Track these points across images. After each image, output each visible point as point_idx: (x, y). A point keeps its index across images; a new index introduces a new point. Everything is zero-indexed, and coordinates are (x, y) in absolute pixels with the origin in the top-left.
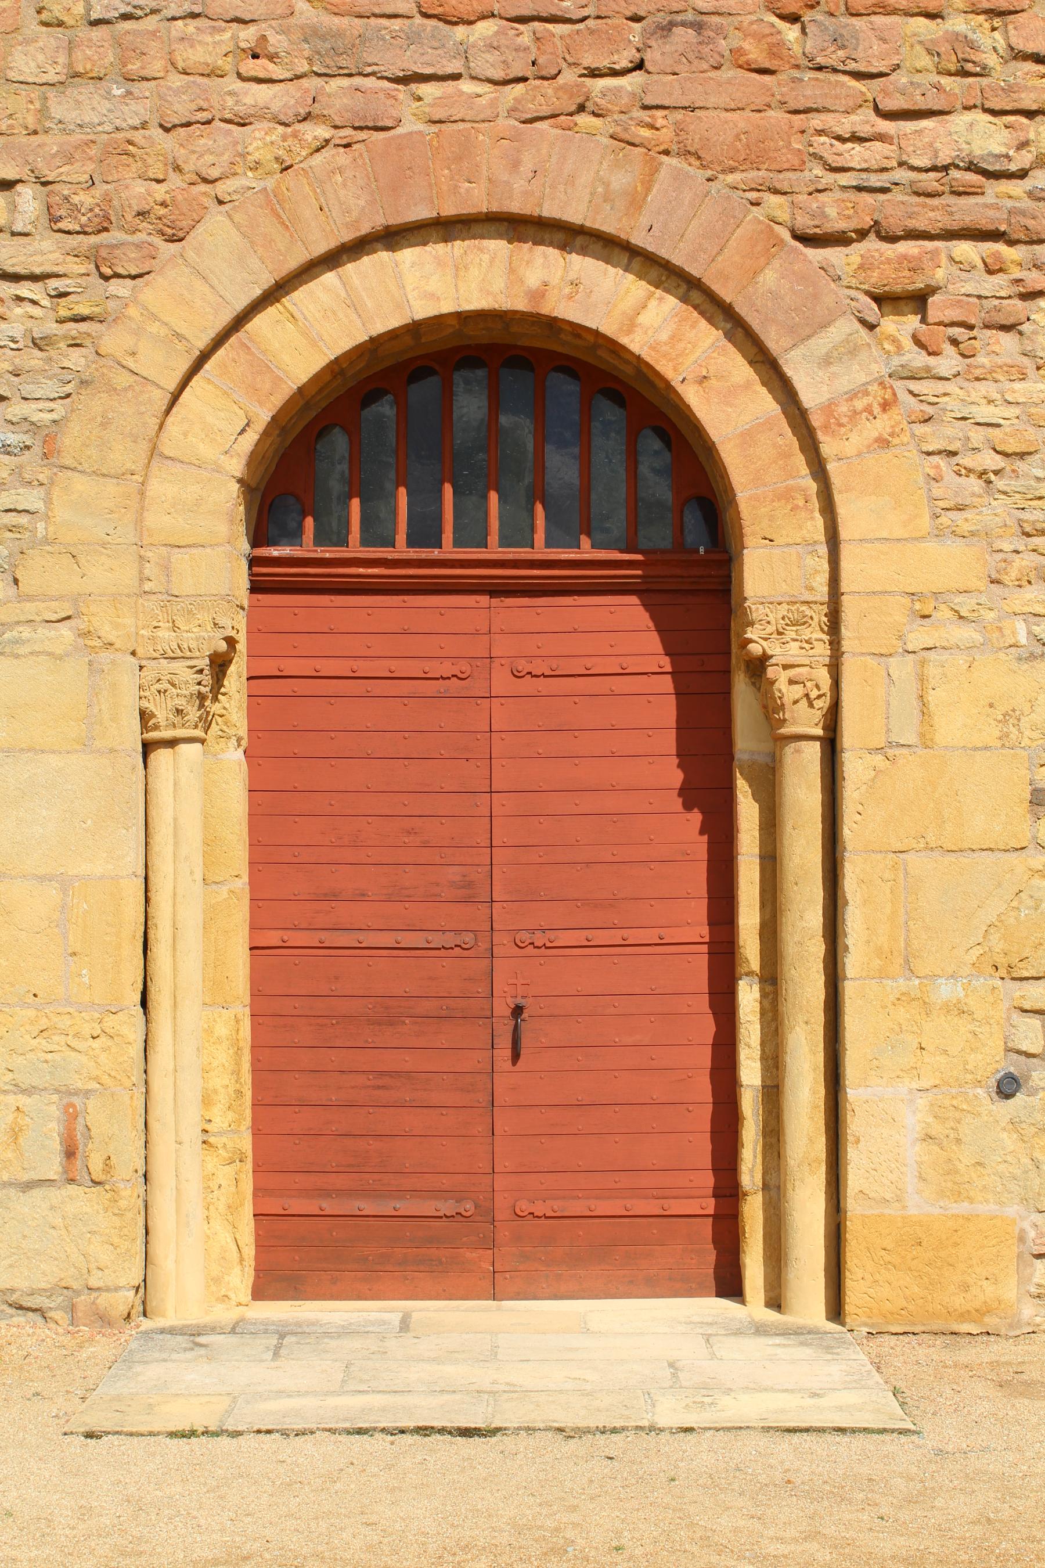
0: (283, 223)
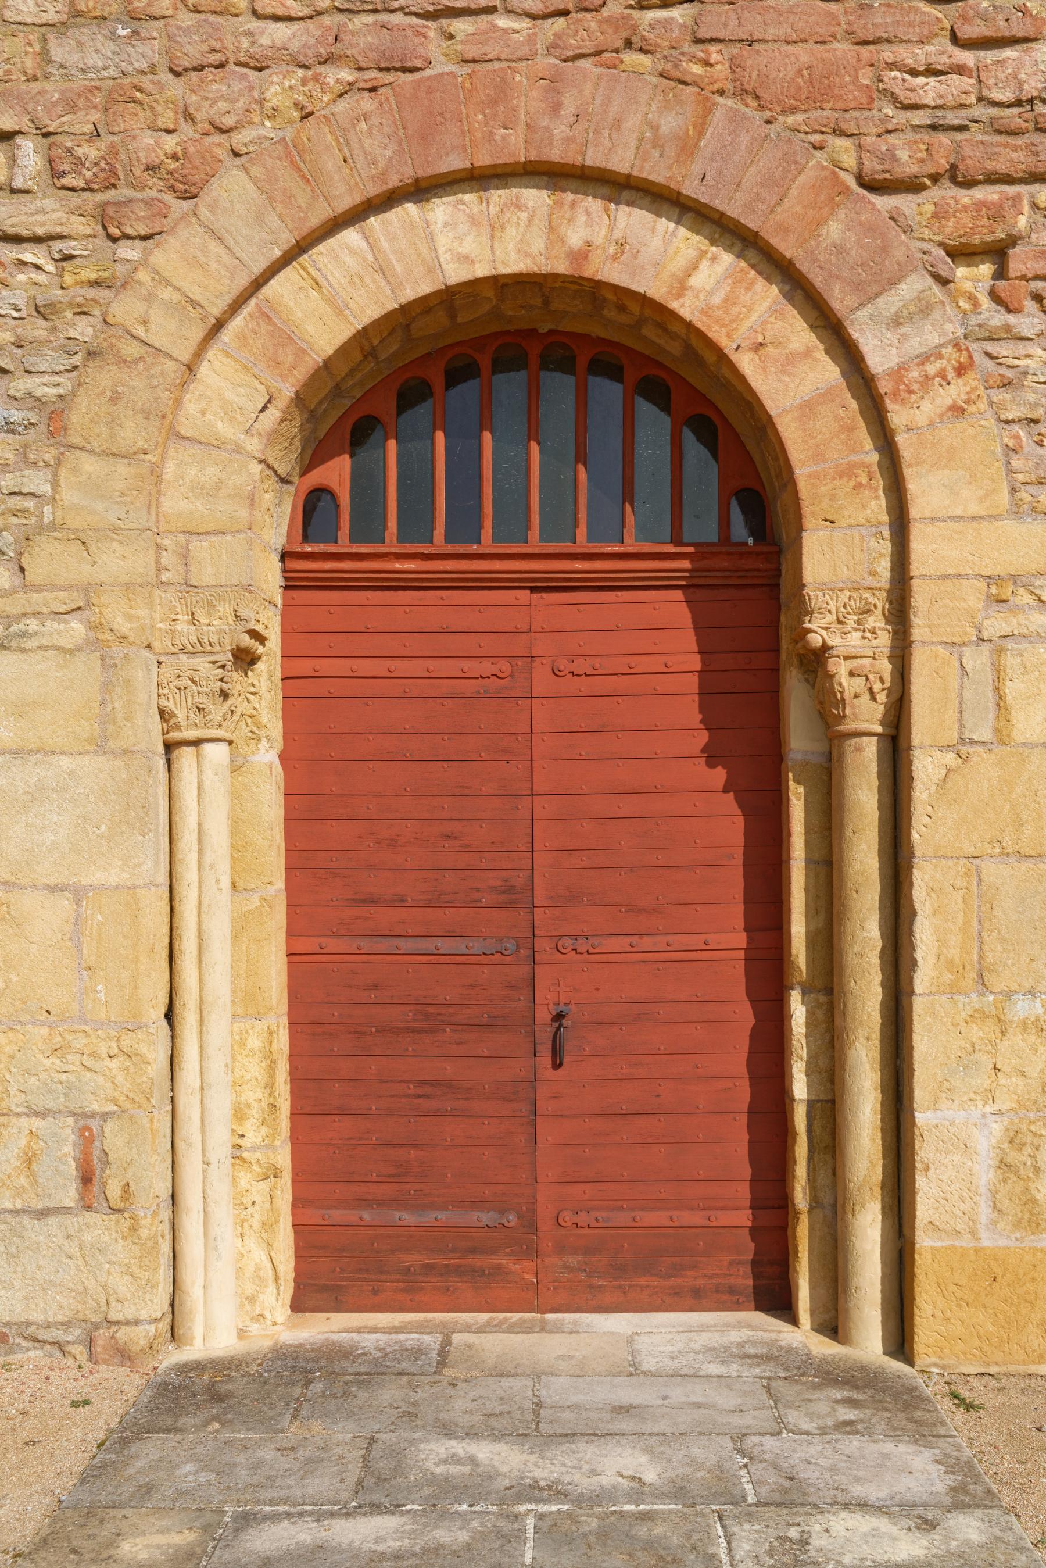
0: (304, 177)
